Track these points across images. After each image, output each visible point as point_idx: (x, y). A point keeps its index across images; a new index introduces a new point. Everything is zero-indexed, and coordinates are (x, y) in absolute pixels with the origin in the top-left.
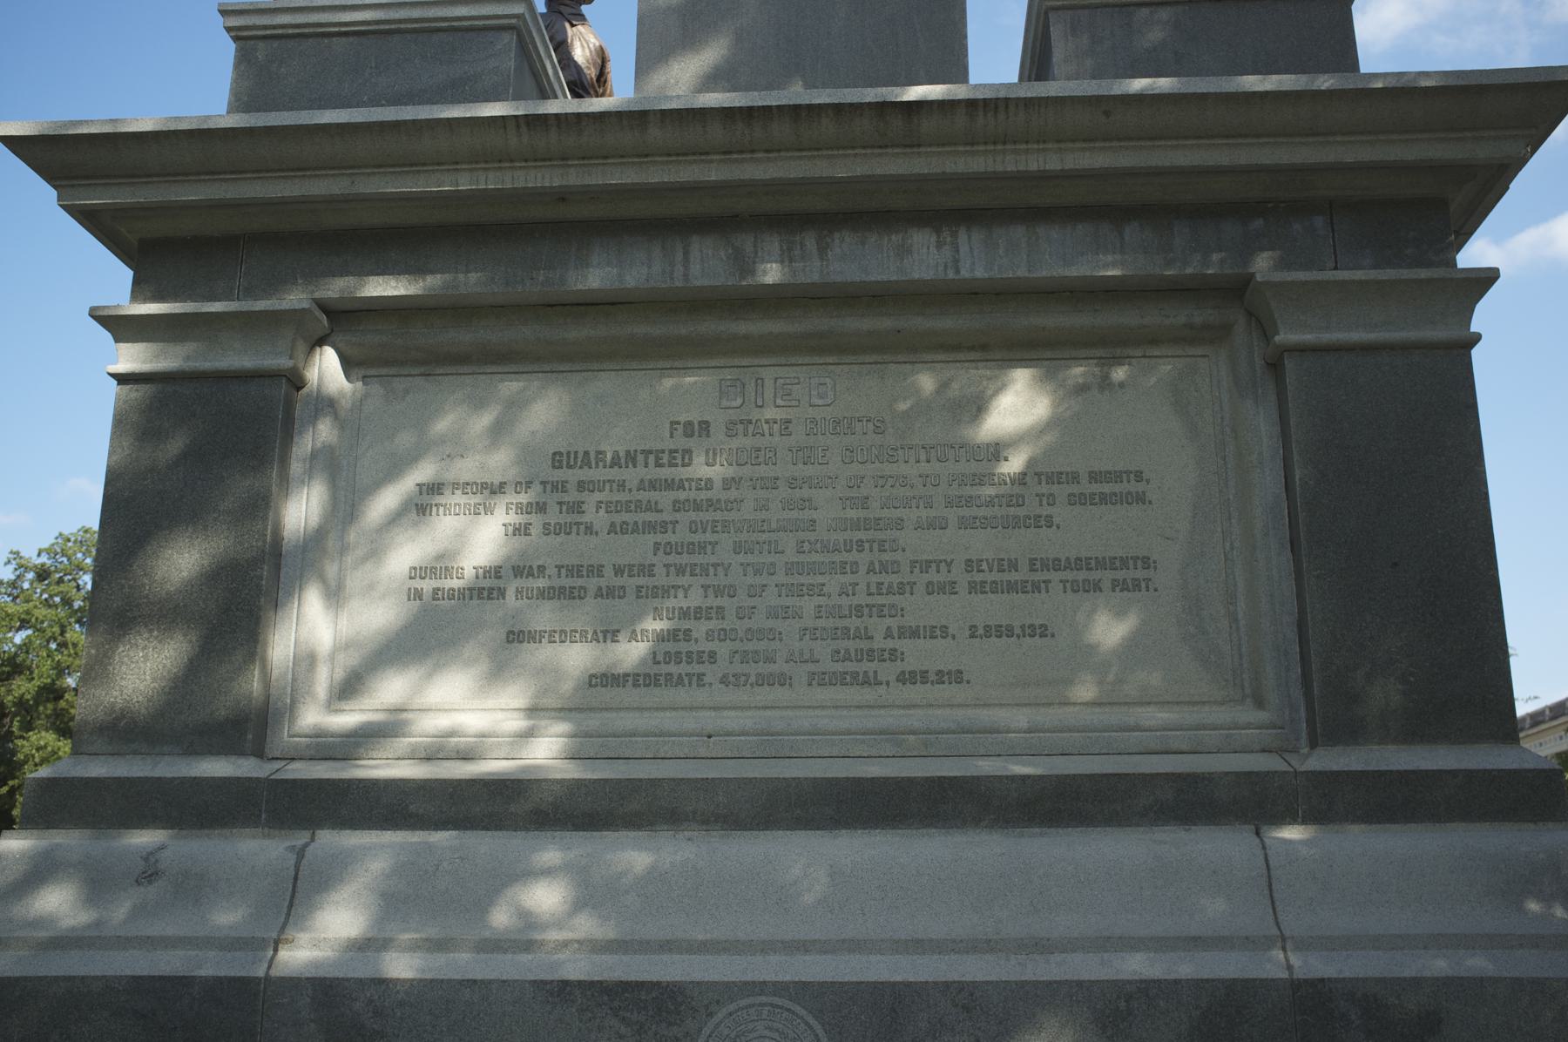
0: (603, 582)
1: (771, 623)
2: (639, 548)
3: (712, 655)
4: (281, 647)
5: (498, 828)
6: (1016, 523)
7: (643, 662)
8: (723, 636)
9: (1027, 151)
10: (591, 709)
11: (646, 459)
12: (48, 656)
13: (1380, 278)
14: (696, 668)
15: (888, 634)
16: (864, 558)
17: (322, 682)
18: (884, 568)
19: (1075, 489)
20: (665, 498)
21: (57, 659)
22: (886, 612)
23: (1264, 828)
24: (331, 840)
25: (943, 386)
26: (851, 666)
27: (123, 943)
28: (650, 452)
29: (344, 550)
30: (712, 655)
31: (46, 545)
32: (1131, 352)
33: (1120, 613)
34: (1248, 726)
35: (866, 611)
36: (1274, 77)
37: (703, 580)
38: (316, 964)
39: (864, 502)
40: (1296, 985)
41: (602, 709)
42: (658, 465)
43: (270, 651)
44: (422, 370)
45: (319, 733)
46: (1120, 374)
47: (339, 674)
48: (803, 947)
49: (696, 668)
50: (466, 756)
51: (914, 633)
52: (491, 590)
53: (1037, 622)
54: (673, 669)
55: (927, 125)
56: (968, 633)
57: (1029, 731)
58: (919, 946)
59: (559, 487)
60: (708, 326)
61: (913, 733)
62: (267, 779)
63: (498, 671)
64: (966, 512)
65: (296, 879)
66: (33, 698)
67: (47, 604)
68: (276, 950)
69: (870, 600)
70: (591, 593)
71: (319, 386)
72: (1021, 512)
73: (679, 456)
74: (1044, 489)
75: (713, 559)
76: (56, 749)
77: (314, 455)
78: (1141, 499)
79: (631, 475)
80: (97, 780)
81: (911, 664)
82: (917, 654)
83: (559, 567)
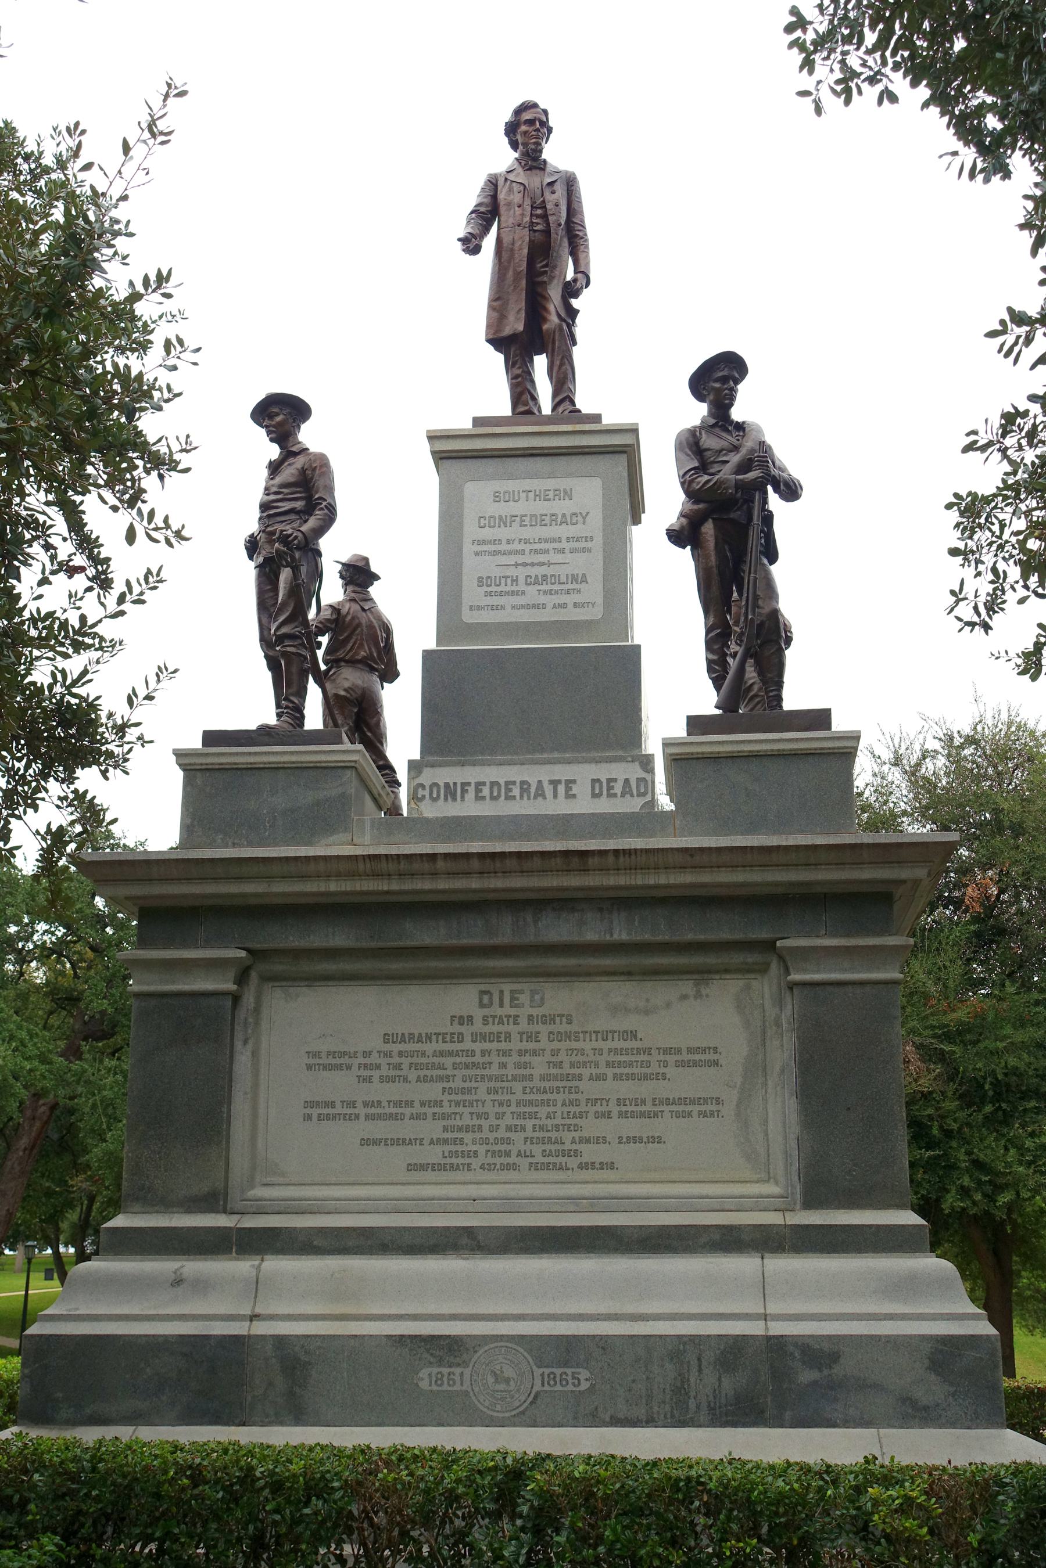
0: (414, 1111)
1: (508, 1135)
3: (476, 1152)
14: (467, 1161)
15: (573, 1142)
16: (560, 1098)
18: (571, 1103)
19: (679, 1057)
22: (572, 1128)
26: (552, 1160)
30: (476, 1152)
32: (714, 976)
35: (561, 1128)
39: (559, 1065)
42: (444, 1042)
49: (467, 1161)
51: (588, 1141)
54: (454, 1161)
59: (388, 1054)
60: (472, 963)
64: (618, 1071)
65: (257, 1283)
69: (563, 1122)
70: (407, 1117)
72: (648, 1071)
74: (662, 1057)
75: (475, 1098)
78: (716, 1063)
81: (586, 1158)
82: (589, 1153)
83: (389, 1102)
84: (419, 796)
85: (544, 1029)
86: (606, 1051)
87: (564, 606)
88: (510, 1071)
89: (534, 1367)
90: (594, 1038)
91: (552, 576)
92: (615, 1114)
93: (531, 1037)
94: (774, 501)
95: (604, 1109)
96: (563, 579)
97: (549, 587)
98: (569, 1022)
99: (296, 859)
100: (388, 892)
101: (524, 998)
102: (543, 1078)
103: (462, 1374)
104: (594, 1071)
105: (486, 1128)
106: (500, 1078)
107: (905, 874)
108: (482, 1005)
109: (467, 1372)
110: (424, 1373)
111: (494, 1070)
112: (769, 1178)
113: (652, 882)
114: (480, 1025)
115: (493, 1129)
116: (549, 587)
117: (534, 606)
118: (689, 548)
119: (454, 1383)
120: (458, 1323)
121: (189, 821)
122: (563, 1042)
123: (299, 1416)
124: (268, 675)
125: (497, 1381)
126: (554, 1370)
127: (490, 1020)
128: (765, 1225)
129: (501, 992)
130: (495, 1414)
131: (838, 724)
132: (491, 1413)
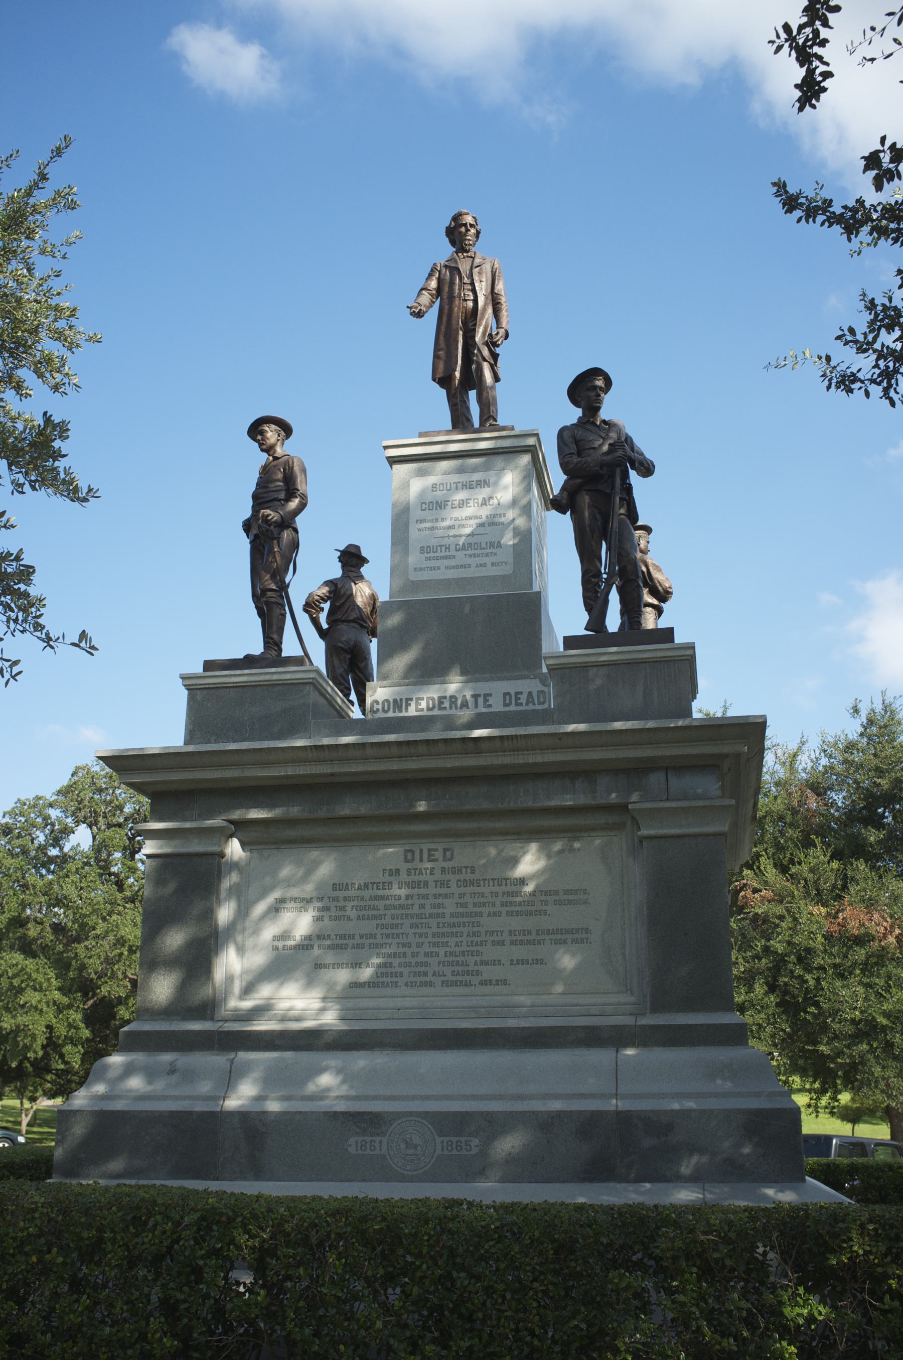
0: (355, 942)
1: (426, 959)
2: (369, 927)
3: (401, 973)
4: (219, 974)
5: (311, 1050)
6: (530, 914)
7: (372, 977)
8: (408, 965)
9: (528, 754)
10: (351, 998)
11: (373, 886)
12: (14, 895)
13: (683, 806)
14: (395, 979)
16: (465, 930)
17: (237, 987)
18: (474, 934)
19: (557, 898)
20: (381, 904)
21: (21, 897)
22: (475, 954)
23: (620, 1049)
24: (244, 1056)
25: (500, 852)
26: (459, 978)
27: (165, 1098)
28: (374, 883)
29: (244, 930)
30: (401, 973)
31: (8, 809)
33: (573, 955)
34: (625, 1004)
35: (466, 953)
36: (631, 722)
37: (397, 940)
38: (242, 1106)
39: (465, 905)
40: (618, 1113)
41: (355, 998)
42: (378, 889)
43: (215, 975)
44: (275, 846)
45: (236, 1010)
46: (577, 845)
47: (244, 984)
48: (428, 1098)
49: (395, 979)
50: (298, 1019)
52: (307, 945)
53: (539, 957)
54: (384, 979)
55: (484, 746)
56: (509, 963)
57: (532, 1006)
58: (465, 1097)
59: (336, 899)
61: (483, 1008)
62: (217, 1031)
63: (310, 983)
64: (510, 909)
65: (230, 1072)
66: (5, 927)
67: (11, 853)
68: (224, 1101)
69: (468, 949)
70: (350, 946)
71: (231, 859)
72: (533, 908)
73: (387, 885)
74: (543, 898)
75: (401, 931)
76: (24, 967)
77: (231, 888)
78: (586, 902)
79: (367, 894)
80: (148, 1031)
81: (485, 976)
82: (488, 972)
83: (336, 935)
84: (375, 709)
85: (453, 878)
86: (500, 895)
87: (484, 565)
88: (428, 910)
89: (436, 1137)
90: (491, 884)
91: (475, 543)
92: (507, 943)
93: (444, 884)
94: (634, 477)
95: (499, 938)
96: (483, 545)
97: (473, 552)
98: (473, 872)
99: (261, 750)
100: (332, 775)
101: (438, 855)
102: (452, 915)
103: (381, 1142)
104: (492, 910)
105: (409, 955)
106: (419, 916)
107: (726, 749)
108: (406, 861)
109: (385, 1140)
110: (352, 1140)
111: (416, 910)
112: (627, 991)
113: (531, 761)
114: (405, 876)
115: (414, 955)
116: (473, 552)
117: (462, 566)
118: (569, 513)
119: (375, 1149)
120: (379, 1102)
121: (191, 727)
122: (468, 888)
123: (258, 1173)
124: (259, 621)
125: (407, 1148)
126: (452, 1138)
127: (413, 871)
128: (620, 1026)
129: (421, 851)
130: (406, 1173)
131: (679, 639)
132: (403, 1172)
